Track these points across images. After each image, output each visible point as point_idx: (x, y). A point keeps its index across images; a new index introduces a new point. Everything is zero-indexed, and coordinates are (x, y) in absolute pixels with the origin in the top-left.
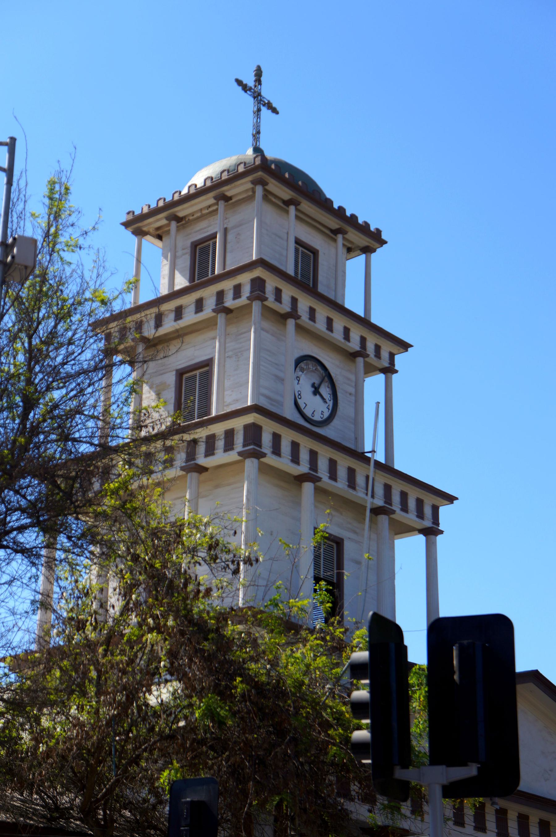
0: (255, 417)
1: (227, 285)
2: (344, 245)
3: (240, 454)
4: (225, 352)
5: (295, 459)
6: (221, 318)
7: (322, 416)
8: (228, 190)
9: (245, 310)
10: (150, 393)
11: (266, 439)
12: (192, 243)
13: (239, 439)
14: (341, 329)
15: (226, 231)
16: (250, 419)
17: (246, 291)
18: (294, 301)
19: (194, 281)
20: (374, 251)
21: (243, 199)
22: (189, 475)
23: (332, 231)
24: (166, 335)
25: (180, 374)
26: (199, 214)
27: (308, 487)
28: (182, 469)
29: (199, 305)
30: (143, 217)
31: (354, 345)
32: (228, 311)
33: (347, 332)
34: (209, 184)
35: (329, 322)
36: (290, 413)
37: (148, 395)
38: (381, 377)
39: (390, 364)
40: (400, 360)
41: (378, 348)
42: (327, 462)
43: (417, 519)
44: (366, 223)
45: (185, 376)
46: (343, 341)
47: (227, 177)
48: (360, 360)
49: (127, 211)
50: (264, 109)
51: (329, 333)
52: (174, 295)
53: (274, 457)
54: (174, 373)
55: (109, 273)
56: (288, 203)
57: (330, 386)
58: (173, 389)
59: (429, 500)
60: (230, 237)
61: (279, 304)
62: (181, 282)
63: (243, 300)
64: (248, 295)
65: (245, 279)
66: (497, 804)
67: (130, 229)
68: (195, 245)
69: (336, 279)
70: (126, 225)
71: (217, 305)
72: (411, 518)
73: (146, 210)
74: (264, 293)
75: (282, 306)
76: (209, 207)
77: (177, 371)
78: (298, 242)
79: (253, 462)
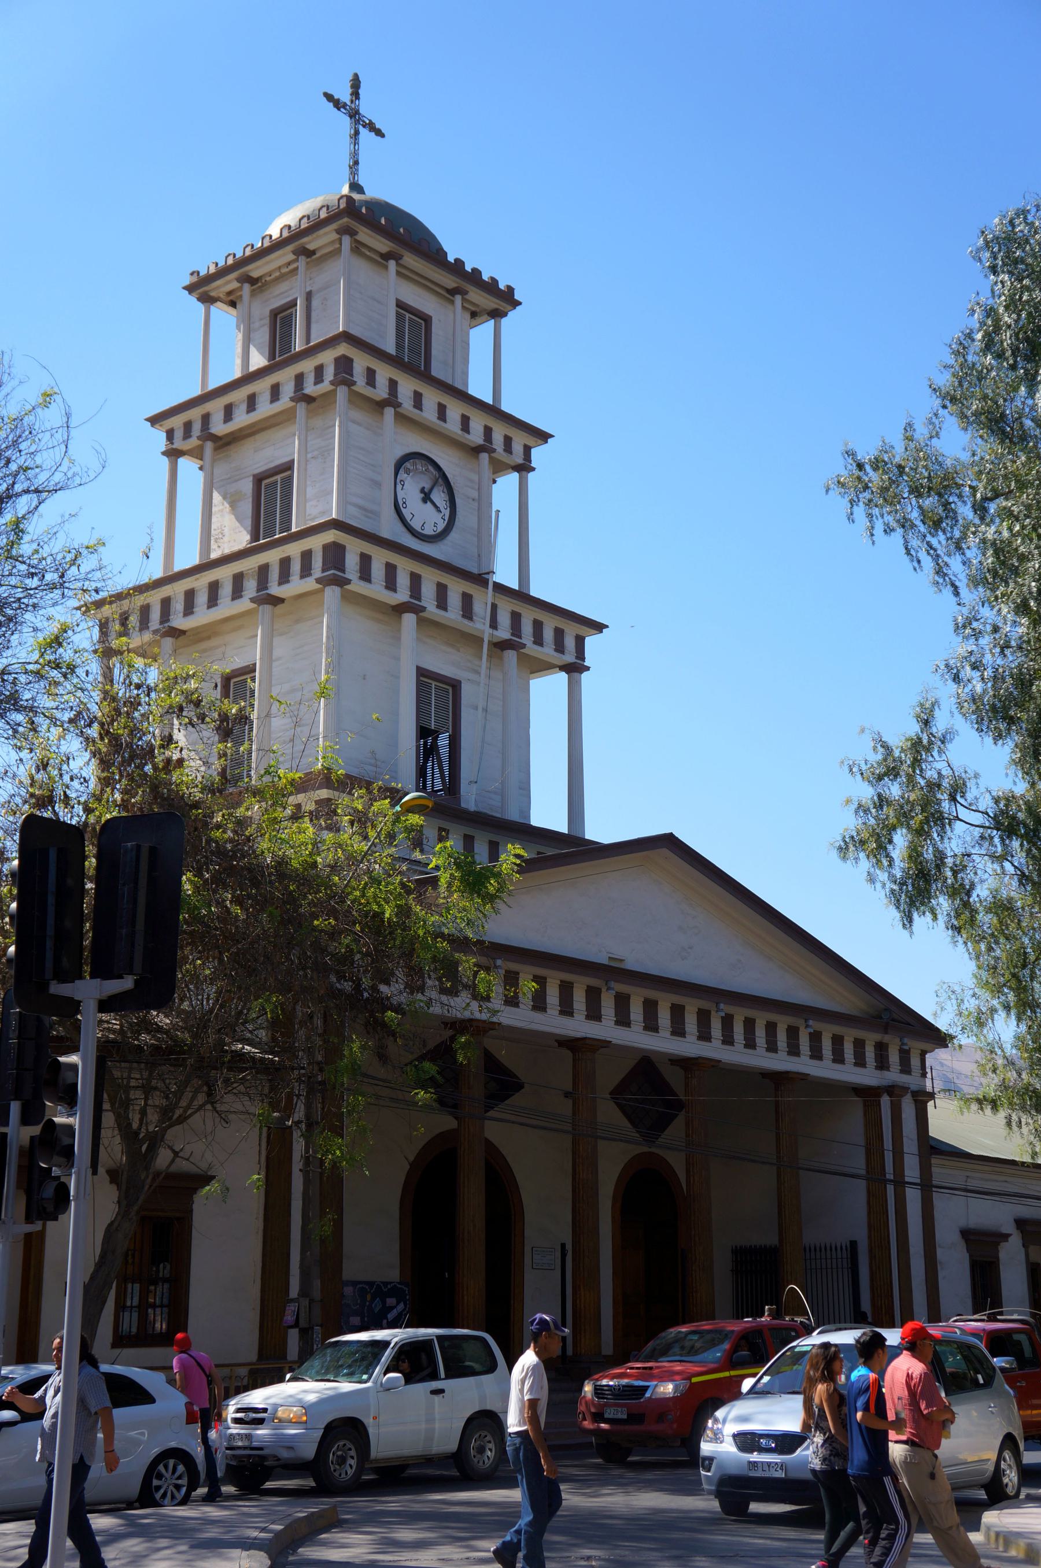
0: (335, 534)
1: (307, 366)
2: (463, 307)
3: (318, 581)
4: (307, 452)
5: (391, 584)
6: (301, 408)
7: (435, 529)
8: (310, 242)
9: (328, 397)
10: (223, 504)
11: (352, 562)
12: (271, 311)
13: (317, 562)
14: (458, 418)
15: (309, 296)
16: (330, 536)
17: (329, 374)
18: (393, 384)
19: (274, 358)
20: (505, 315)
21: (331, 252)
22: (261, 608)
23: (448, 291)
24: (241, 430)
25: (258, 480)
26: (277, 274)
27: (409, 620)
28: (252, 600)
29: (275, 392)
30: (210, 279)
31: (476, 436)
32: (309, 399)
33: (465, 421)
34: (286, 234)
35: (442, 410)
36: (388, 527)
37: (221, 507)
38: (515, 476)
39: (524, 459)
40: (538, 454)
41: (508, 441)
42: (435, 587)
43: (556, 654)
44: (492, 279)
45: (264, 483)
46: (460, 432)
47: (307, 225)
48: (484, 456)
49: (191, 271)
50: (364, 132)
51: (442, 423)
52: (249, 378)
53: (362, 583)
54: (251, 478)
55: (16, 382)
56: (387, 256)
57: (445, 490)
58: (250, 500)
59: (571, 630)
60: (315, 303)
61: (372, 389)
62: (258, 360)
63: (325, 386)
64: (332, 378)
65: (327, 358)
66: (613, 989)
67: (196, 294)
68: (275, 314)
69: (454, 352)
70: (190, 289)
71: (295, 392)
72: (547, 651)
73: (212, 270)
74: (352, 375)
75: (377, 391)
76: (289, 264)
77: (254, 476)
78: (400, 305)
79: (333, 591)
